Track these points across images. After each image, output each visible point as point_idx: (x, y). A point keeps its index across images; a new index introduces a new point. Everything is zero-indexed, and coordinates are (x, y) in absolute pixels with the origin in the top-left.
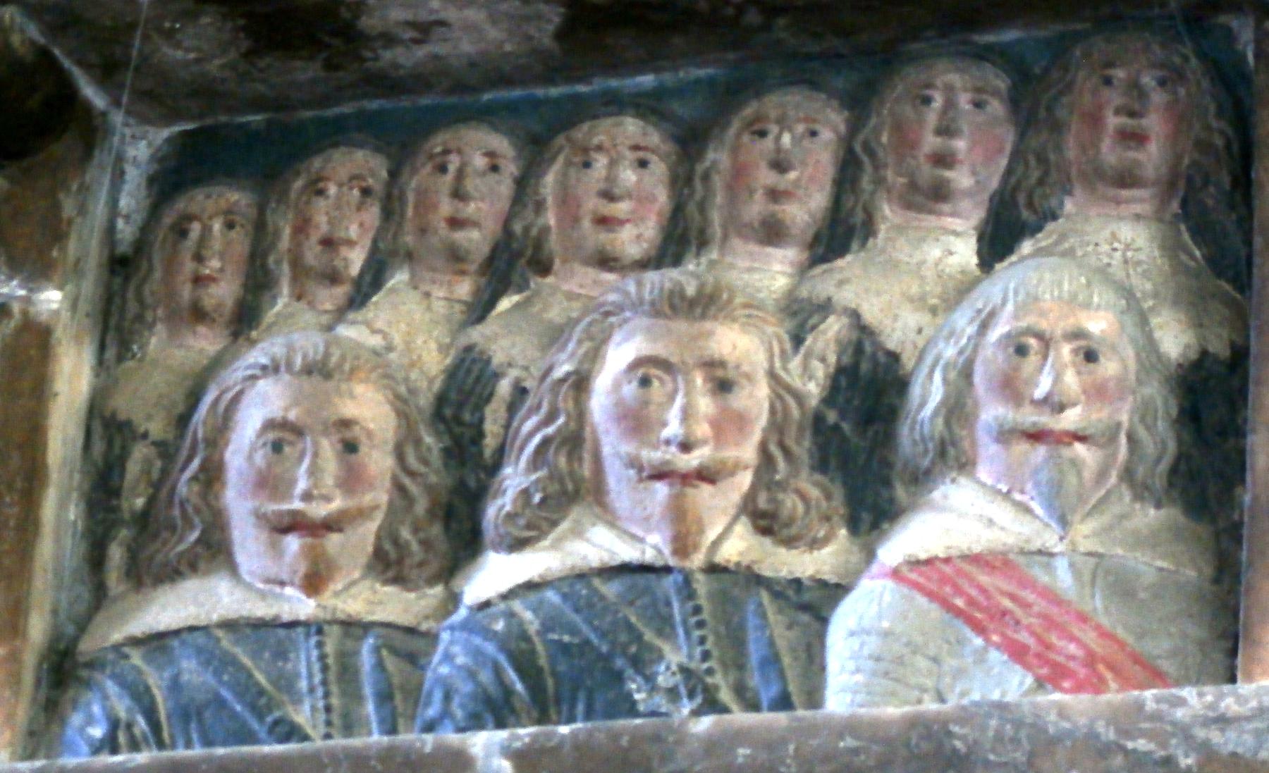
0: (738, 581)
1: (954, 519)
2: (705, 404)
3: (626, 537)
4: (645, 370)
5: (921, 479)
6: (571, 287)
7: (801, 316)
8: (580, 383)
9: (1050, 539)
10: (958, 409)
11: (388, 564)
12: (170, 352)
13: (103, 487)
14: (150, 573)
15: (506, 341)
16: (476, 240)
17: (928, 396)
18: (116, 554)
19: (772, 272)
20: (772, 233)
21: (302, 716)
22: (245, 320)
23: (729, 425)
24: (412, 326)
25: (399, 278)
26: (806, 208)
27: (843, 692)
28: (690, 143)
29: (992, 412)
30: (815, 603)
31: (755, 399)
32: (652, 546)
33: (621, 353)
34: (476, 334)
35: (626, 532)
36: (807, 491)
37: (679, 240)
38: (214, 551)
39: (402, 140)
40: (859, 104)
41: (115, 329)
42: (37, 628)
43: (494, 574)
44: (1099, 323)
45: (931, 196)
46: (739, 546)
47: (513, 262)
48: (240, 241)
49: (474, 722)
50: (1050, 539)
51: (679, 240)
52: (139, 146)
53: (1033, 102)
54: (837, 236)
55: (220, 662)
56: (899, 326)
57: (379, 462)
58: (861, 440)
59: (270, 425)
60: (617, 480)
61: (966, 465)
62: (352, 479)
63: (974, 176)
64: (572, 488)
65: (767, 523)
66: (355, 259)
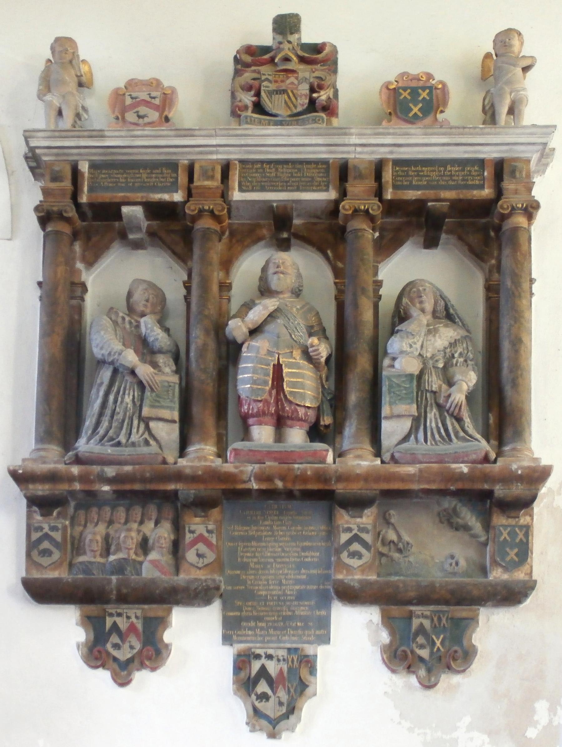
0: (134, 561)
1: (153, 556)
2: (131, 541)
3: (159, 138)
4: (125, 537)
5: (150, 551)
6: (116, 526)
7: (139, 531)
8: (119, 538)
9: (162, 558)
10: (153, 543)
11: (101, 555)
12: (78, 529)
13: (73, 544)
14: (79, 554)
15: (111, 532)
16: (108, 519)
17: (151, 542)
18: (75, 552)
19: (135, 526)
20: (135, 521)
21: (95, 572)
22: (85, 526)
23: (133, 543)
24: (101, 529)
25: (100, 523)
26: (139, 519)
27: (144, 575)
28: (128, 510)
29: (157, 544)
30: (141, 563)
31: (135, 540)
32: (125, 556)
33: (123, 535)
34: (108, 530)
35: (116, 331)
36: (140, 551)
37: (126, 522)
38: (85, 553)
39: (100, 507)
40: (143, 507)
41: (72, 524)
42: (68, 560)
43: (112, 558)
44: (166, 535)
45: (150, 519)
46: (134, 557)
47: (111, 523)
48: (84, 517)
49: (112, 573)
50: (162, 558)
51: (126, 522)
52: (73, 504)
53: (159, 511)
54: (141, 523)
55: (86, 566)
56: (148, 534)
57: (100, 544)
58: (144, 546)
59: (90, 540)
60: (123, 549)
61: (154, 549)
62: (98, 546)
63: (154, 516)
64: (119, 549)
65: (136, 554)
66: (96, 520)
